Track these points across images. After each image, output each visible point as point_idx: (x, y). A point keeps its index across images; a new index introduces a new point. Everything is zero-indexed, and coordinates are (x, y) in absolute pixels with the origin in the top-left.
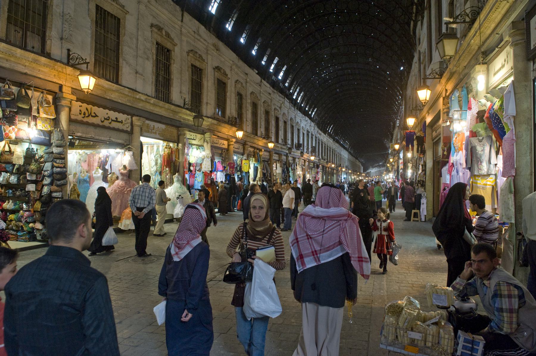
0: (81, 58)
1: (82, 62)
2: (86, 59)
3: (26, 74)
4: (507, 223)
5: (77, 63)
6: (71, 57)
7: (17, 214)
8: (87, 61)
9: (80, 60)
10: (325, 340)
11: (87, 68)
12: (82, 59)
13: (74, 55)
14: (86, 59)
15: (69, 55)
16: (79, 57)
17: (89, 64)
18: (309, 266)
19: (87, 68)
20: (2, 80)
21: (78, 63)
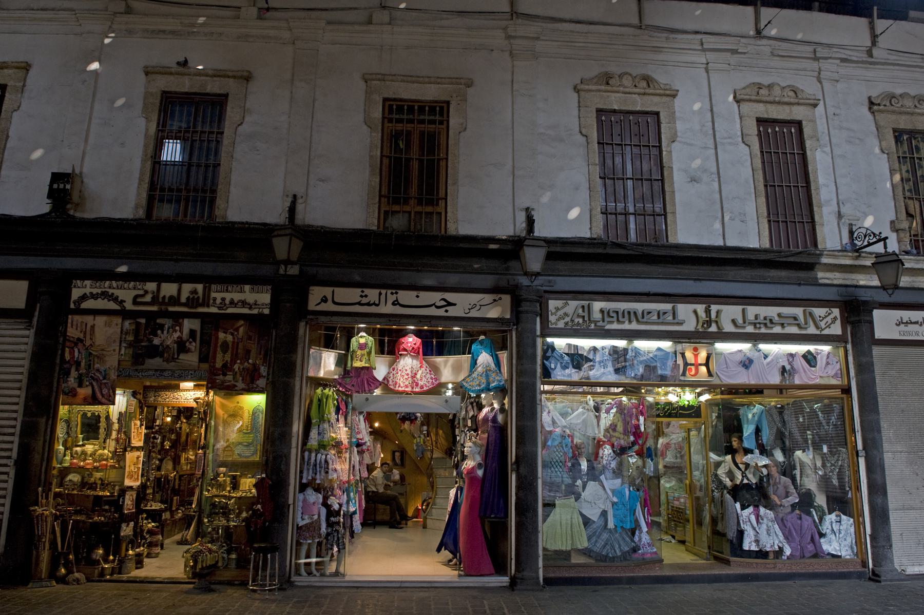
0: (872, 233)
1: (875, 240)
2: (880, 233)
3: (144, 38)
4: (413, 518)
5: (866, 243)
6: (855, 235)
7: (649, 436)
8: (883, 236)
9: (871, 238)
10: (729, 35)
11: (885, 247)
12: (874, 234)
13: (860, 230)
14: (880, 233)
15: (851, 233)
16: (869, 232)
17: (887, 241)
18: (710, 330)
19: (885, 247)
20: (2, 68)
21: (868, 242)
